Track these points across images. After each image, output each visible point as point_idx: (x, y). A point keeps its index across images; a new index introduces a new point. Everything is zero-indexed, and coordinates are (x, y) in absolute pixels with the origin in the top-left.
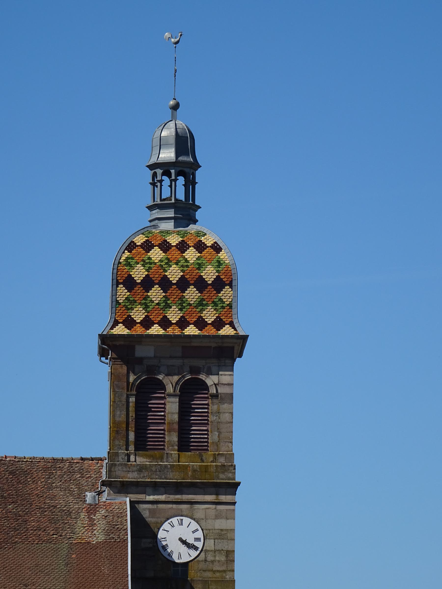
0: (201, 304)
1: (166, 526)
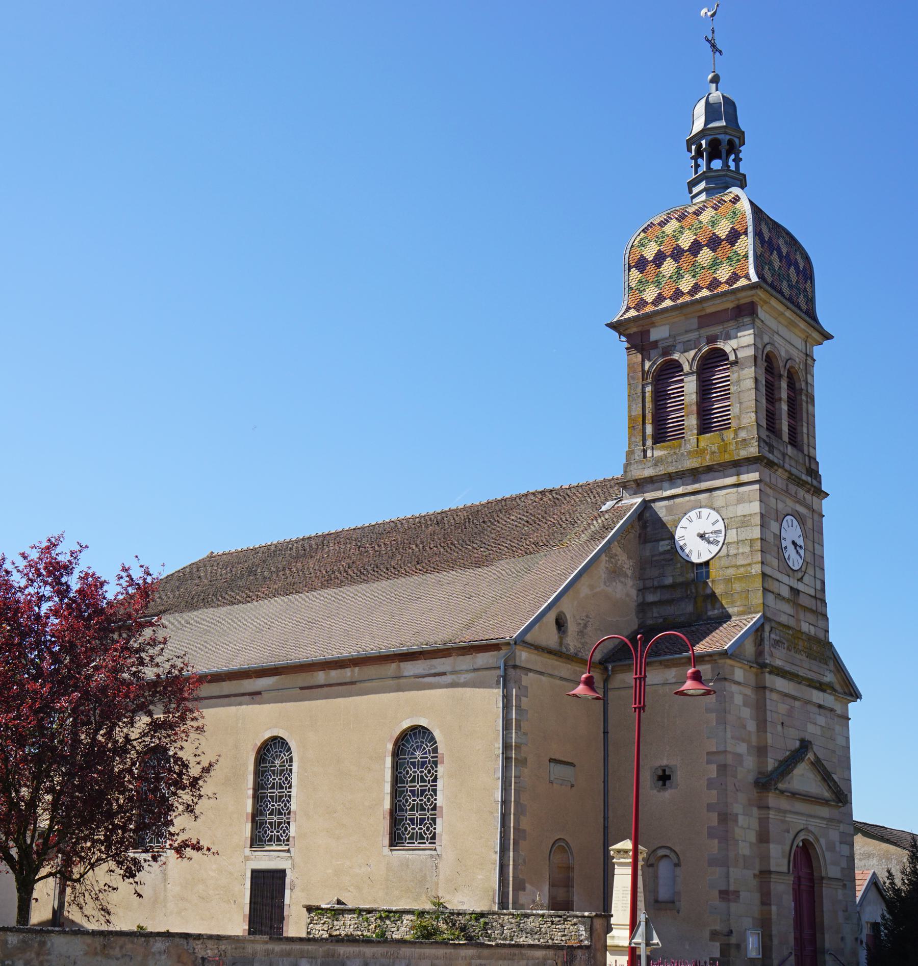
0: (715, 264)
1: (684, 522)
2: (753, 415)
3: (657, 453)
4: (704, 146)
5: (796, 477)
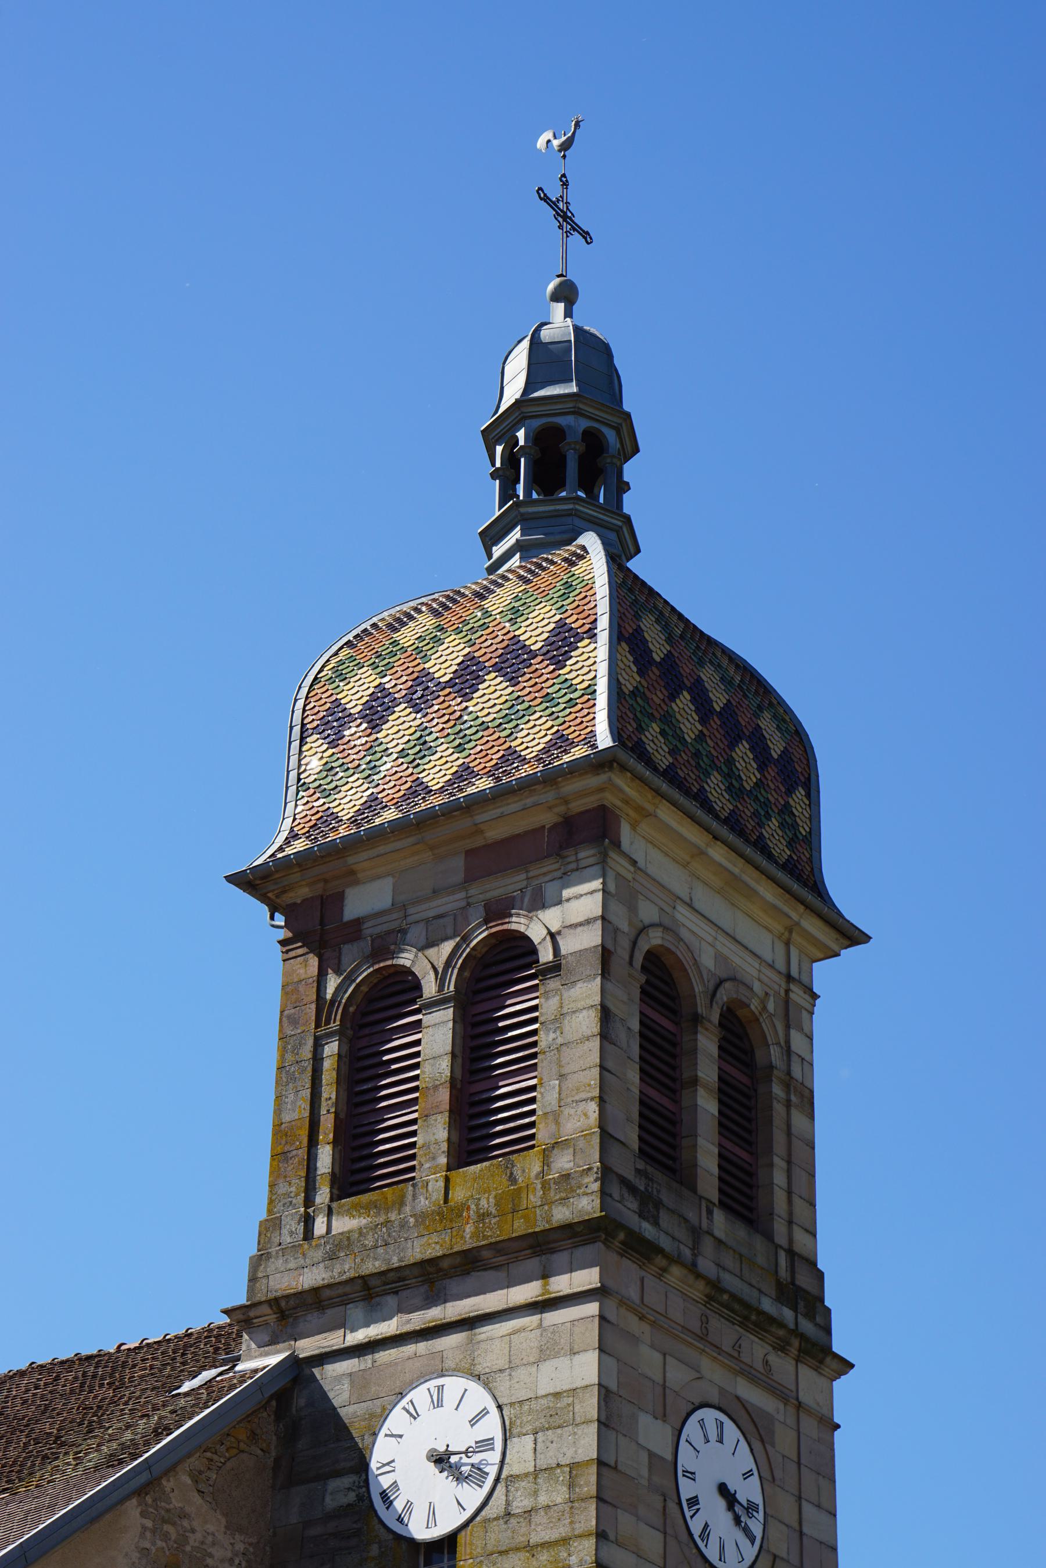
0: (514, 714)
1: (397, 1420)
2: (593, 1108)
3: (342, 1224)
4: (522, 443)
5: (733, 1296)
